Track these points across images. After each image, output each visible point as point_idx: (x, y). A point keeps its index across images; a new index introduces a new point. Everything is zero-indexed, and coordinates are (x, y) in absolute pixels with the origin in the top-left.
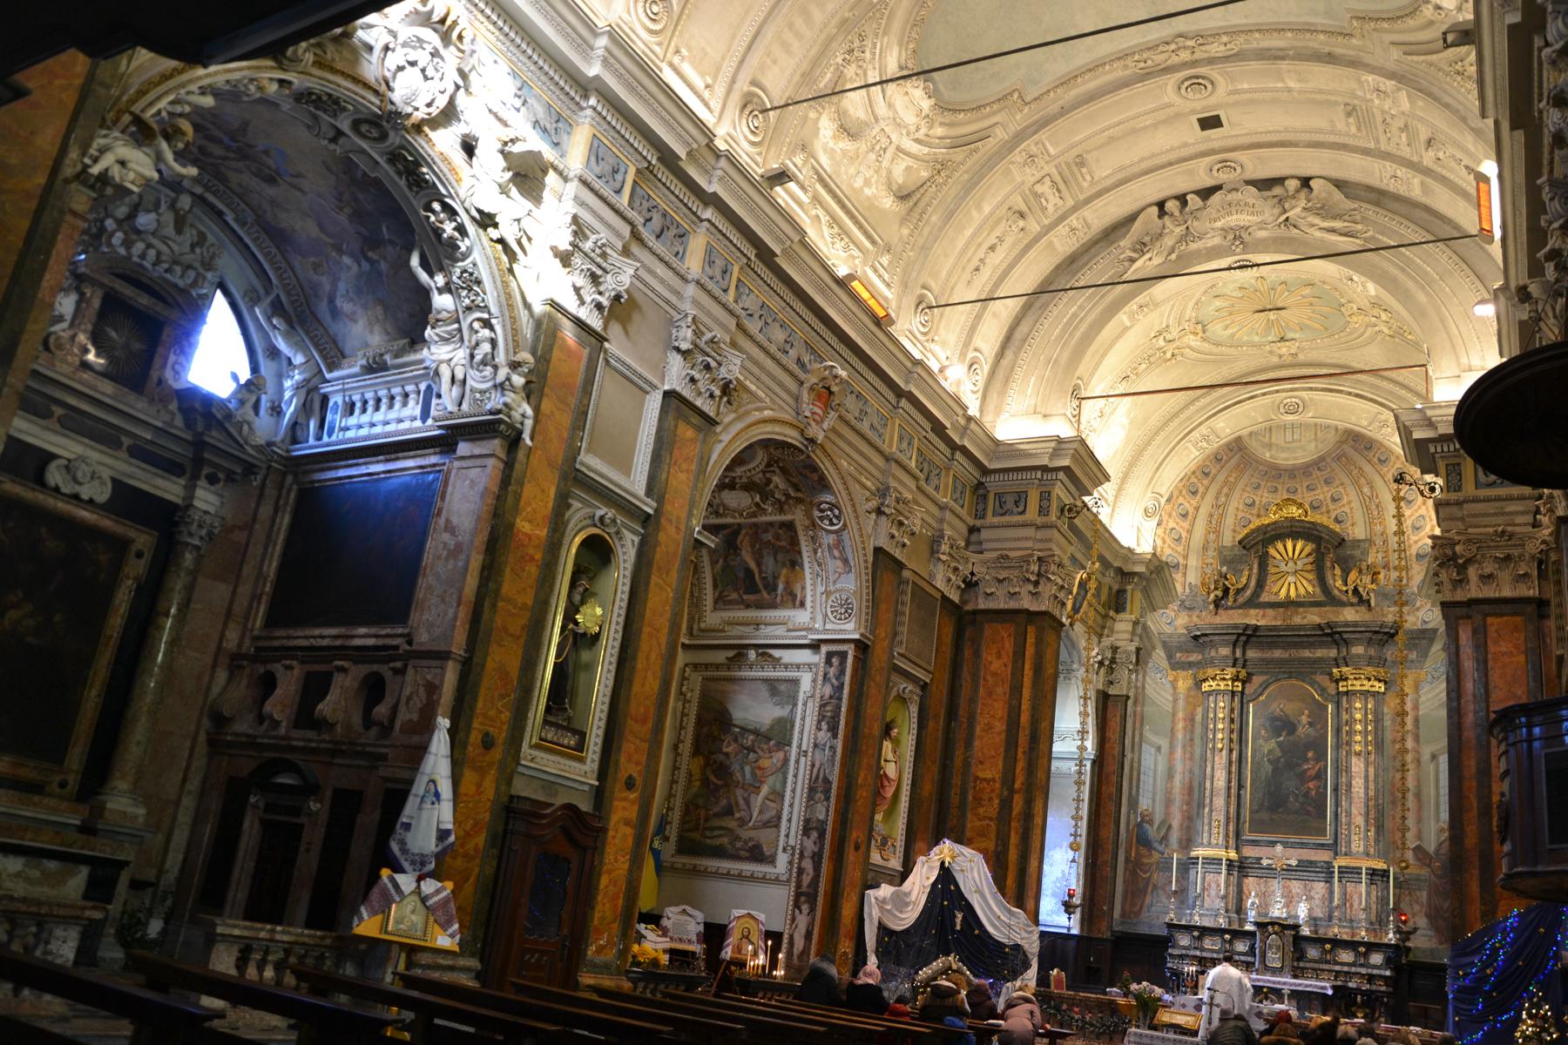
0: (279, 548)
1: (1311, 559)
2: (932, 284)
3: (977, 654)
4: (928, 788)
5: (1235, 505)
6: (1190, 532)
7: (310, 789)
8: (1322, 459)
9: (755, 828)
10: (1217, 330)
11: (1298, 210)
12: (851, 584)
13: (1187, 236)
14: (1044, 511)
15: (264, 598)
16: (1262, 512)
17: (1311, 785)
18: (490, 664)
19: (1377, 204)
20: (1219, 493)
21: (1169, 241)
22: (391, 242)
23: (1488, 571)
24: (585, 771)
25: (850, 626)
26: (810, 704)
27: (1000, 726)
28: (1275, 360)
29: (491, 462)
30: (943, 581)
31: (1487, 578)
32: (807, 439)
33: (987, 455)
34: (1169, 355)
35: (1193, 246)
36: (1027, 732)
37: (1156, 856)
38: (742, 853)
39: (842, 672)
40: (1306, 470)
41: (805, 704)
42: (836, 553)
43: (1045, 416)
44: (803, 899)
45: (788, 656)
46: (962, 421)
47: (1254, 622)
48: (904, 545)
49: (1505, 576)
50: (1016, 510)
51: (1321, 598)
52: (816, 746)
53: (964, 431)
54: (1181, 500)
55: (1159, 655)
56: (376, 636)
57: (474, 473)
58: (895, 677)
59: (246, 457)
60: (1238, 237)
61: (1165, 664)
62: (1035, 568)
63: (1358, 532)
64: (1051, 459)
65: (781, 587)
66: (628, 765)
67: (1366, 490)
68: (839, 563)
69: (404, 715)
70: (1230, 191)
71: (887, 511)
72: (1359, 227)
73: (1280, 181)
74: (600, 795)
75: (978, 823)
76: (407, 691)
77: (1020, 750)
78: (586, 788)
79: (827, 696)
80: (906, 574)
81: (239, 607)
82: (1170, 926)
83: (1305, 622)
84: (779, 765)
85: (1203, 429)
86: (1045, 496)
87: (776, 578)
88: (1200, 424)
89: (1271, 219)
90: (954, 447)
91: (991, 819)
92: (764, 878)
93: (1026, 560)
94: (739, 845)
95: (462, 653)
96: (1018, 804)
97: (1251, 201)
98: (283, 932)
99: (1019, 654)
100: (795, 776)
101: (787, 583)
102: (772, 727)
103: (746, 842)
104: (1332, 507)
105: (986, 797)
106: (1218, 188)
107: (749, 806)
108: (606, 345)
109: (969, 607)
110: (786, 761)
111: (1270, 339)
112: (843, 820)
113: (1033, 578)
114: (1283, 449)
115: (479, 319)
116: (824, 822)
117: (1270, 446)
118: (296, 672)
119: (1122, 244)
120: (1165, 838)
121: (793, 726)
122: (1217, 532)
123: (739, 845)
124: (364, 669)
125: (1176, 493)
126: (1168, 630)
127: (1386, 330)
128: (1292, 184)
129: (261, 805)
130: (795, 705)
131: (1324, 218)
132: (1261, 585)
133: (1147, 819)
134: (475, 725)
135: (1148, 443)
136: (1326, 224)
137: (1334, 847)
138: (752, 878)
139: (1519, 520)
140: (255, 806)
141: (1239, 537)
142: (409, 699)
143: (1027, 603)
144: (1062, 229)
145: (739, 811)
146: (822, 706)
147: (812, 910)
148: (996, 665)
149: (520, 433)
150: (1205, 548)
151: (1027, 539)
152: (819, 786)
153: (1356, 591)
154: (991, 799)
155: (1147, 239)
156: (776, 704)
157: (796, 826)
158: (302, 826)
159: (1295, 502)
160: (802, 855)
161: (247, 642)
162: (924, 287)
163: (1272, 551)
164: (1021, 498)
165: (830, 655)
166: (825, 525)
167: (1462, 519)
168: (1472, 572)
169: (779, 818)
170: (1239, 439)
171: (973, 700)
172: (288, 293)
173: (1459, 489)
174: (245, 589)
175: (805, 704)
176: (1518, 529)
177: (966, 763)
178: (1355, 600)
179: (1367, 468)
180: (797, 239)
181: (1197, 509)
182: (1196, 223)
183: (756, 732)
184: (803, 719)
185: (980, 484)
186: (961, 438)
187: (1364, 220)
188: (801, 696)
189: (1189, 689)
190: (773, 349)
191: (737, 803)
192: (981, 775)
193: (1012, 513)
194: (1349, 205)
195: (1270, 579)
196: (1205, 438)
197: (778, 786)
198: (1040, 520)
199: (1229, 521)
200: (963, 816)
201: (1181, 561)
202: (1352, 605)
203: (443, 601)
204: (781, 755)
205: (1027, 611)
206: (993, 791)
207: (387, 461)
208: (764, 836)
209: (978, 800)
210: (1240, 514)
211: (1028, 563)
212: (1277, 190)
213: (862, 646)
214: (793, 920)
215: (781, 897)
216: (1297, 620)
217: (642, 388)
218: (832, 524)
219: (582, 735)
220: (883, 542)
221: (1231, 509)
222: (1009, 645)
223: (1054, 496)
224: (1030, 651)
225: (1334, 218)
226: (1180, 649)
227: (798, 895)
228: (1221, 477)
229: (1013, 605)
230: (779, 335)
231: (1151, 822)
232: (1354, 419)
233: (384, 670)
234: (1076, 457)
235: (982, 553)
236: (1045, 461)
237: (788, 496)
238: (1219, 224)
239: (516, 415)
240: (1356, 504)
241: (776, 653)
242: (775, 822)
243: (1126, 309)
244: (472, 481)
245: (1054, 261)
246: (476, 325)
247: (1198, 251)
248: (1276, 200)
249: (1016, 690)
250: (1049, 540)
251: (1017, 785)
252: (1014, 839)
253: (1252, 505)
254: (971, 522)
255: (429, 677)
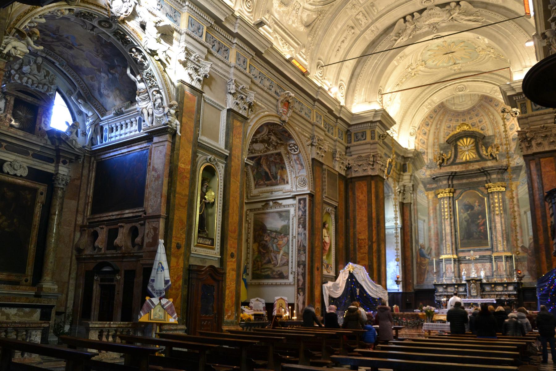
0: (92, 185)
1: (473, 145)
2: (322, 57)
3: (354, 194)
4: (341, 244)
5: (444, 127)
6: (427, 140)
7: (116, 271)
8: (474, 107)
9: (280, 267)
10: (430, 63)
11: (456, 14)
12: (304, 173)
13: (415, 29)
14: (373, 138)
15: (90, 204)
16: (454, 129)
17: (481, 228)
18: (176, 218)
19: (486, 8)
20: (437, 124)
21: (409, 31)
22: (119, 66)
23: (539, 142)
24: (215, 253)
25: (306, 188)
26: (294, 219)
27: (365, 219)
28: (453, 72)
29: (166, 143)
30: (339, 168)
31: (539, 144)
32: (282, 121)
33: (349, 119)
34: (413, 74)
35: (418, 32)
36: (375, 220)
37: (427, 260)
38: (277, 276)
39: (305, 206)
40: (468, 112)
41: (293, 219)
42: (298, 162)
43: (369, 102)
44: (300, 290)
45: (284, 202)
46: (339, 108)
47: (455, 170)
48: (322, 156)
49: (546, 143)
50: (362, 139)
51: (478, 159)
52: (298, 234)
53: (340, 111)
54: (423, 128)
55: (421, 187)
56: (133, 213)
57: (161, 148)
58: (325, 206)
59: (74, 152)
60: (434, 27)
61: (423, 189)
62: (372, 159)
63: (490, 133)
64: (373, 118)
65: (279, 177)
66: (231, 248)
67: (491, 117)
68: (299, 166)
69: (146, 240)
70: (430, 10)
71: (315, 144)
72: (480, 18)
73: (448, 4)
74: (222, 261)
75: (361, 256)
76: (147, 231)
77: (374, 227)
78: (216, 259)
79: (300, 215)
80: (324, 167)
81: (80, 209)
82: (435, 285)
83: (473, 168)
84: (286, 243)
85: (429, 101)
86: (373, 132)
87: (276, 174)
88: (427, 99)
89: (446, 18)
90: (337, 118)
91: (366, 253)
92: (285, 284)
93: (368, 157)
94: (274, 273)
95: (165, 215)
96: (375, 246)
97: (438, 12)
98: (113, 324)
99: (369, 191)
100: (292, 246)
101: (281, 176)
102: (281, 229)
103: (277, 272)
104: (479, 124)
105: (363, 245)
106: (425, 9)
107: (276, 258)
108: (204, 94)
109: (349, 177)
110: (288, 241)
111: (450, 64)
112: (312, 260)
113: (372, 163)
114: (459, 105)
115: (155, 91)
116: (305, 261)
117: (454, 104)
118: (105, 230)
119: (391, 34)
120: (430, 253)
121: (289, 228)
122: (438, 139)
123: (274, 273)
124: (129, 226)
125: (421, 126)
126: (423, 177)
127: (493, 56)
128: (453, 4)
129: (99, 279)
130: (289, 220)
131: (466, 16)
132: (456, 156)
133: (423, 247)
134: (173, 241)
135: (409, 108)
136: (467, 18)
137: (492, 250)
138: (281, 285)
139: (549, 121)
140: (97, 280)
141: (446, 140)
142: (148, 234)
143: (370, 173)
144: (368, 31)
145: (273, 261)
146: (299, 219)
147: (304, 294)
148: (361, 197)
149: (176, 131)
150: (434, 145)
151: (368, 149)
152: (301, 249)
153: (491, 155)
154: (365, 246)
155: (400, 32)
156: (282, 220)
157: (295, 264)
158: (115, 285)
159: (465, 124)
160: (298, 274)
161: (85, 221)
162: (319, 59)
163: (459, 143)
164: (364, 134)
165: (300, 200)
166: (293, 152)
167: (528, 123)
168: (533, 143)
169: (288, 262)
170: (442, 103)
171: (354, 211)
172: (83, 90)
173: (526, 112)
174: (82, 202)
175: (293, 219)
176: (549, 125)
177: (354, 234)
178: (491, 158)
179: (491, 109)
180: (269, 46)
181: (429, 131)
182: (418, 23)
183: (276, 232)
184: (293, 225)
185: (348, 131)
186: (339, 114)
187: (482, 15)
188: (291, 217)
189: (433, 198)
190: (266, 89)
191: (272, 258)
192: (360, 238)
193: (361, 140)
194: (475, 10)
195: (459, 154)
196: (430, 104)
197: (287, 251)
198: (372, 141)
199: (442, 134)
200: (355, 253)
201: (426, 151)
202: (490, 160)
203: (156, 197)
204: (286, 239)
205: (371, 176)
206: (365, 243)
207: (128, 148)
208: (283, 269)
209: (360, 247)
210: (446, 131)
211: (369, 158)
212: (448, 7)
213: (311, 195)
214: (298, 298)
215: (292, 290)
216: (471, 168)
217: (219, 109)
218: (295, 151)
219: (213, 240)
220: (315, 156)
221: (442, 130)
222: (365, 189)
223: (376, 132)
224: (373, 190)
225: (470, 15)
226: (429, 183)
227: (298, 289)
228: (437, 118)
229: (365, 174)
230: (267, 83)
231: (424, 248)
232: (484, 91)
233: (137, 225)
234: (383, 116)
235: (351, 156)
236: (371, 119)
237: (277, 143)
238: (427, 23)
239: (174, 125)
240: (488, 123)
241: (280, 202)
242: (287, 264)
243: (395, 59)
244: (160, 151)
245: (367, 44)
246: (154, 93)
247: (420, 34)
248: (447, 11)
249: (370, 205)
250: (376, 148)
251: (374, 240)
252: (375, 260)
253: (449, 127)
254: (346, 145)
255: (154, 225)
